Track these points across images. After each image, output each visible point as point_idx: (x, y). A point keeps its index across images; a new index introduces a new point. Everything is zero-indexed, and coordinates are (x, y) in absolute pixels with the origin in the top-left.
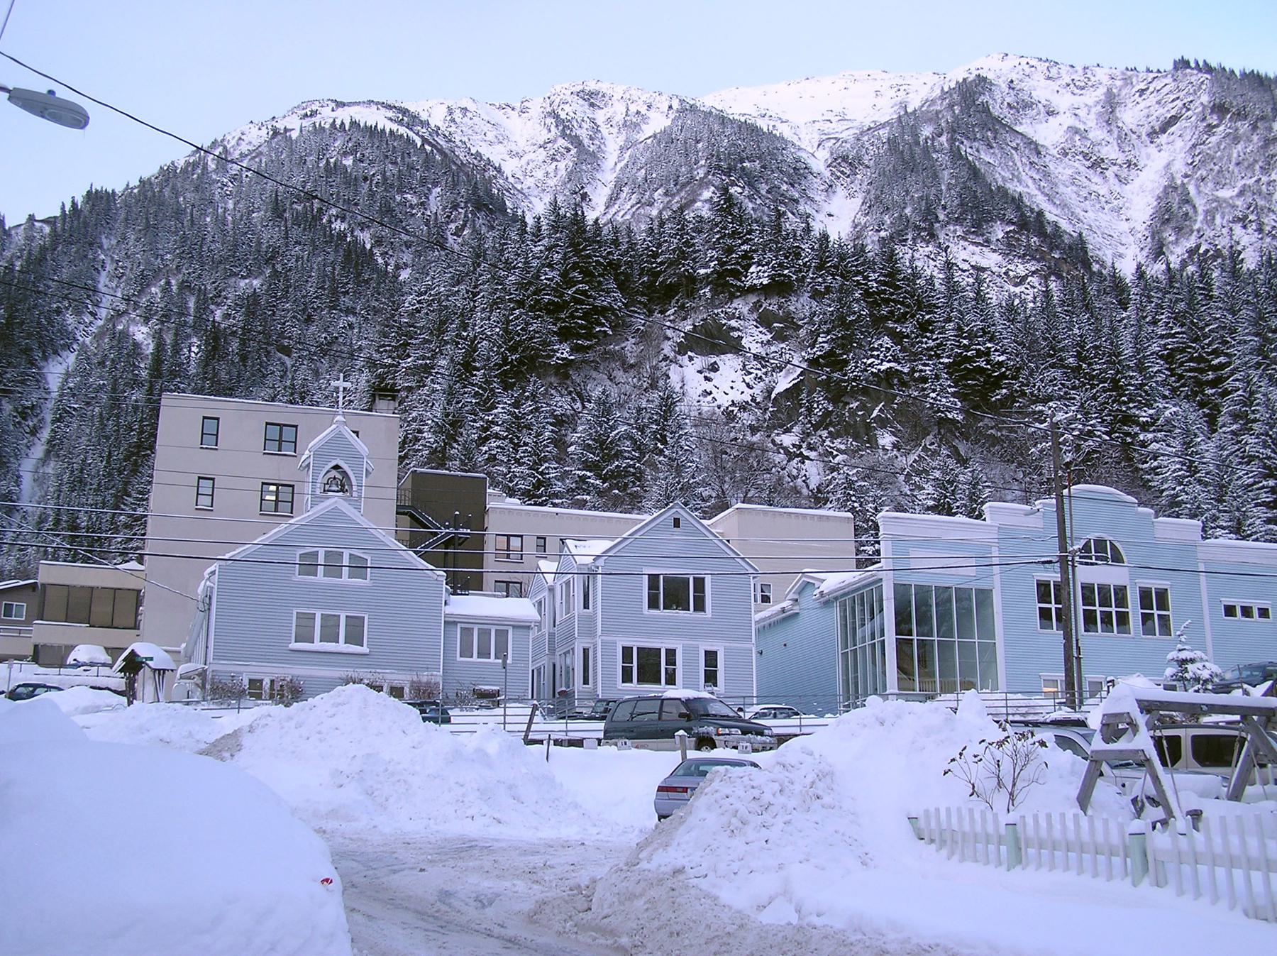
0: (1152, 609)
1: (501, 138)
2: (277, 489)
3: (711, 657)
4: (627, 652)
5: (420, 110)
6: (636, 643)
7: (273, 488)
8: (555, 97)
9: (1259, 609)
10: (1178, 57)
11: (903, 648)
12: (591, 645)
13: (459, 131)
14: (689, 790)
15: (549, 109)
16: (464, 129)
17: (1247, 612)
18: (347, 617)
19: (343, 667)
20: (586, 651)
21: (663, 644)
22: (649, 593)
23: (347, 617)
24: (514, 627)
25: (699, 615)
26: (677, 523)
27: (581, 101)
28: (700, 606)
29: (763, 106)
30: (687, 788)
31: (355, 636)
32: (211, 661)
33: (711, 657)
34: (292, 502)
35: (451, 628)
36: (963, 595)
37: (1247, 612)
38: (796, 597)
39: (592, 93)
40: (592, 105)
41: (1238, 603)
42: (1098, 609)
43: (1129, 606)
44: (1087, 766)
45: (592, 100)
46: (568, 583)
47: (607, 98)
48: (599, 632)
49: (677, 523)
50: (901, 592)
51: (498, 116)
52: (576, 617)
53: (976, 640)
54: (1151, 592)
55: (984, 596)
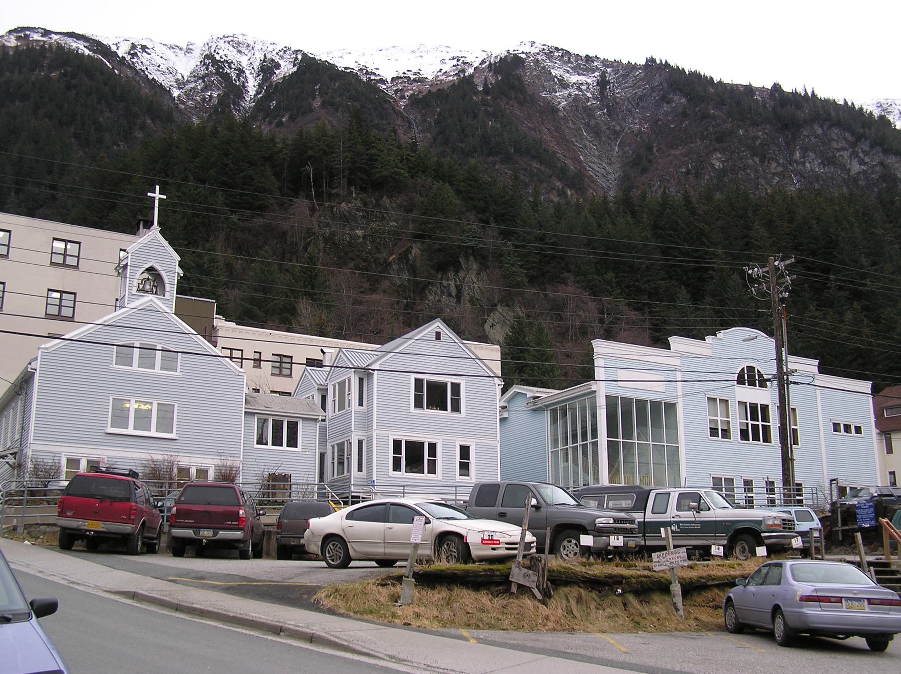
0: (762, 425)
1: (171, 70)
2: (61, 296)
3: (464, 451)
4: (397, 444)
5: (110, 43)
6: (405, 436)
7: (57, 295)
8: (212, 44)
9: (844, 425)
10: (649, 56)
11: (612, 447)
12: (365, 438)
13: (139, 62)
14: (844, 600)
15: (207, 52)
16: (143, 60)
17: (847, 428)
18: (158, 403)
19: (162, 451)
20: (360, 443)
21: (426, 438)
22: (415, 394)
23: (158, 403)
24: (304, 419)
25: (455, 415)
26: (438, 336)
27: (231, 48)
28: (456, 408)
29: (363, 63)
30: (841, 598)
31: (165, 422)
32: (31, 442)
33: (464, 451)
34: (74, 308)
35: (250, 418)
36: (656, 405)
37: (847, 428)
38: (505, 405)
39: (240, 43)
40: (240, 52)
41: (842, 421)
42: (760, 423)
43: (771, 421)
44: (619, 545)
45: (239, 48)
46: (342, 385)
47: (251, 48)
48: (375, 427)
49: (438, 336)
50: (611, 401)
51: (169, 54)
52: (353, 412)
53: (665, 444)
54: (757, 407)
55: (671, 407)
